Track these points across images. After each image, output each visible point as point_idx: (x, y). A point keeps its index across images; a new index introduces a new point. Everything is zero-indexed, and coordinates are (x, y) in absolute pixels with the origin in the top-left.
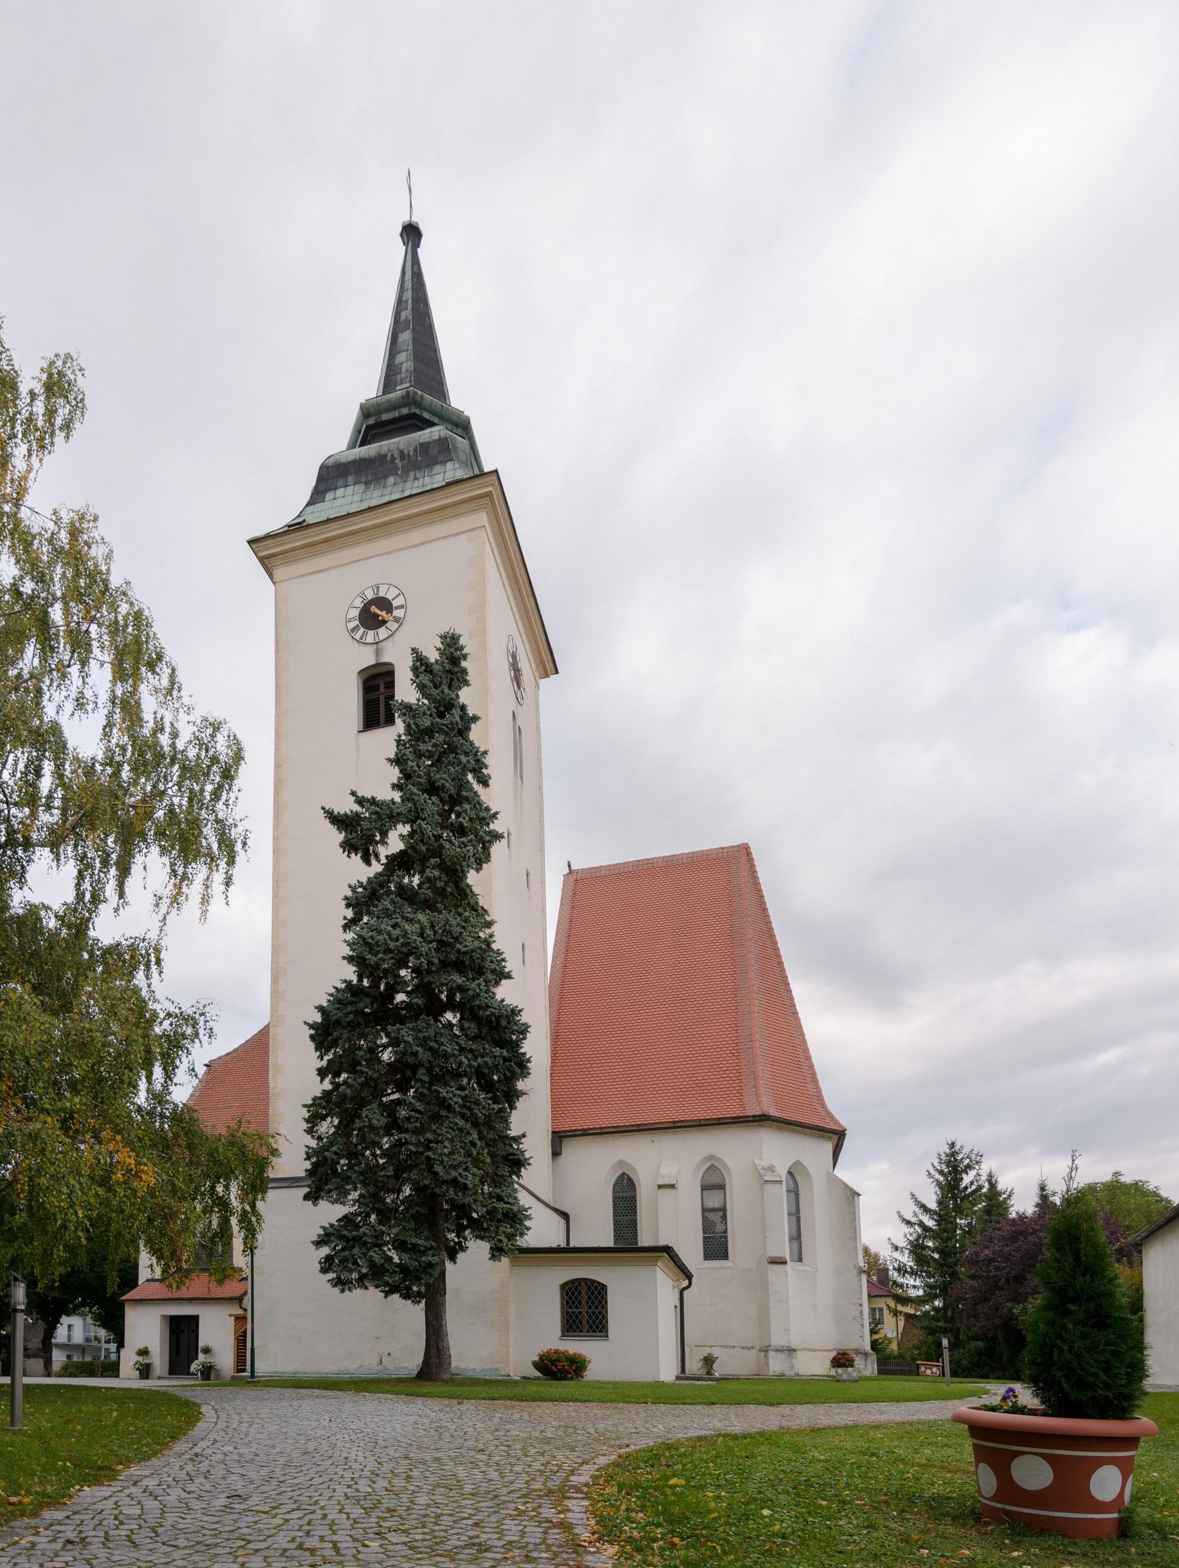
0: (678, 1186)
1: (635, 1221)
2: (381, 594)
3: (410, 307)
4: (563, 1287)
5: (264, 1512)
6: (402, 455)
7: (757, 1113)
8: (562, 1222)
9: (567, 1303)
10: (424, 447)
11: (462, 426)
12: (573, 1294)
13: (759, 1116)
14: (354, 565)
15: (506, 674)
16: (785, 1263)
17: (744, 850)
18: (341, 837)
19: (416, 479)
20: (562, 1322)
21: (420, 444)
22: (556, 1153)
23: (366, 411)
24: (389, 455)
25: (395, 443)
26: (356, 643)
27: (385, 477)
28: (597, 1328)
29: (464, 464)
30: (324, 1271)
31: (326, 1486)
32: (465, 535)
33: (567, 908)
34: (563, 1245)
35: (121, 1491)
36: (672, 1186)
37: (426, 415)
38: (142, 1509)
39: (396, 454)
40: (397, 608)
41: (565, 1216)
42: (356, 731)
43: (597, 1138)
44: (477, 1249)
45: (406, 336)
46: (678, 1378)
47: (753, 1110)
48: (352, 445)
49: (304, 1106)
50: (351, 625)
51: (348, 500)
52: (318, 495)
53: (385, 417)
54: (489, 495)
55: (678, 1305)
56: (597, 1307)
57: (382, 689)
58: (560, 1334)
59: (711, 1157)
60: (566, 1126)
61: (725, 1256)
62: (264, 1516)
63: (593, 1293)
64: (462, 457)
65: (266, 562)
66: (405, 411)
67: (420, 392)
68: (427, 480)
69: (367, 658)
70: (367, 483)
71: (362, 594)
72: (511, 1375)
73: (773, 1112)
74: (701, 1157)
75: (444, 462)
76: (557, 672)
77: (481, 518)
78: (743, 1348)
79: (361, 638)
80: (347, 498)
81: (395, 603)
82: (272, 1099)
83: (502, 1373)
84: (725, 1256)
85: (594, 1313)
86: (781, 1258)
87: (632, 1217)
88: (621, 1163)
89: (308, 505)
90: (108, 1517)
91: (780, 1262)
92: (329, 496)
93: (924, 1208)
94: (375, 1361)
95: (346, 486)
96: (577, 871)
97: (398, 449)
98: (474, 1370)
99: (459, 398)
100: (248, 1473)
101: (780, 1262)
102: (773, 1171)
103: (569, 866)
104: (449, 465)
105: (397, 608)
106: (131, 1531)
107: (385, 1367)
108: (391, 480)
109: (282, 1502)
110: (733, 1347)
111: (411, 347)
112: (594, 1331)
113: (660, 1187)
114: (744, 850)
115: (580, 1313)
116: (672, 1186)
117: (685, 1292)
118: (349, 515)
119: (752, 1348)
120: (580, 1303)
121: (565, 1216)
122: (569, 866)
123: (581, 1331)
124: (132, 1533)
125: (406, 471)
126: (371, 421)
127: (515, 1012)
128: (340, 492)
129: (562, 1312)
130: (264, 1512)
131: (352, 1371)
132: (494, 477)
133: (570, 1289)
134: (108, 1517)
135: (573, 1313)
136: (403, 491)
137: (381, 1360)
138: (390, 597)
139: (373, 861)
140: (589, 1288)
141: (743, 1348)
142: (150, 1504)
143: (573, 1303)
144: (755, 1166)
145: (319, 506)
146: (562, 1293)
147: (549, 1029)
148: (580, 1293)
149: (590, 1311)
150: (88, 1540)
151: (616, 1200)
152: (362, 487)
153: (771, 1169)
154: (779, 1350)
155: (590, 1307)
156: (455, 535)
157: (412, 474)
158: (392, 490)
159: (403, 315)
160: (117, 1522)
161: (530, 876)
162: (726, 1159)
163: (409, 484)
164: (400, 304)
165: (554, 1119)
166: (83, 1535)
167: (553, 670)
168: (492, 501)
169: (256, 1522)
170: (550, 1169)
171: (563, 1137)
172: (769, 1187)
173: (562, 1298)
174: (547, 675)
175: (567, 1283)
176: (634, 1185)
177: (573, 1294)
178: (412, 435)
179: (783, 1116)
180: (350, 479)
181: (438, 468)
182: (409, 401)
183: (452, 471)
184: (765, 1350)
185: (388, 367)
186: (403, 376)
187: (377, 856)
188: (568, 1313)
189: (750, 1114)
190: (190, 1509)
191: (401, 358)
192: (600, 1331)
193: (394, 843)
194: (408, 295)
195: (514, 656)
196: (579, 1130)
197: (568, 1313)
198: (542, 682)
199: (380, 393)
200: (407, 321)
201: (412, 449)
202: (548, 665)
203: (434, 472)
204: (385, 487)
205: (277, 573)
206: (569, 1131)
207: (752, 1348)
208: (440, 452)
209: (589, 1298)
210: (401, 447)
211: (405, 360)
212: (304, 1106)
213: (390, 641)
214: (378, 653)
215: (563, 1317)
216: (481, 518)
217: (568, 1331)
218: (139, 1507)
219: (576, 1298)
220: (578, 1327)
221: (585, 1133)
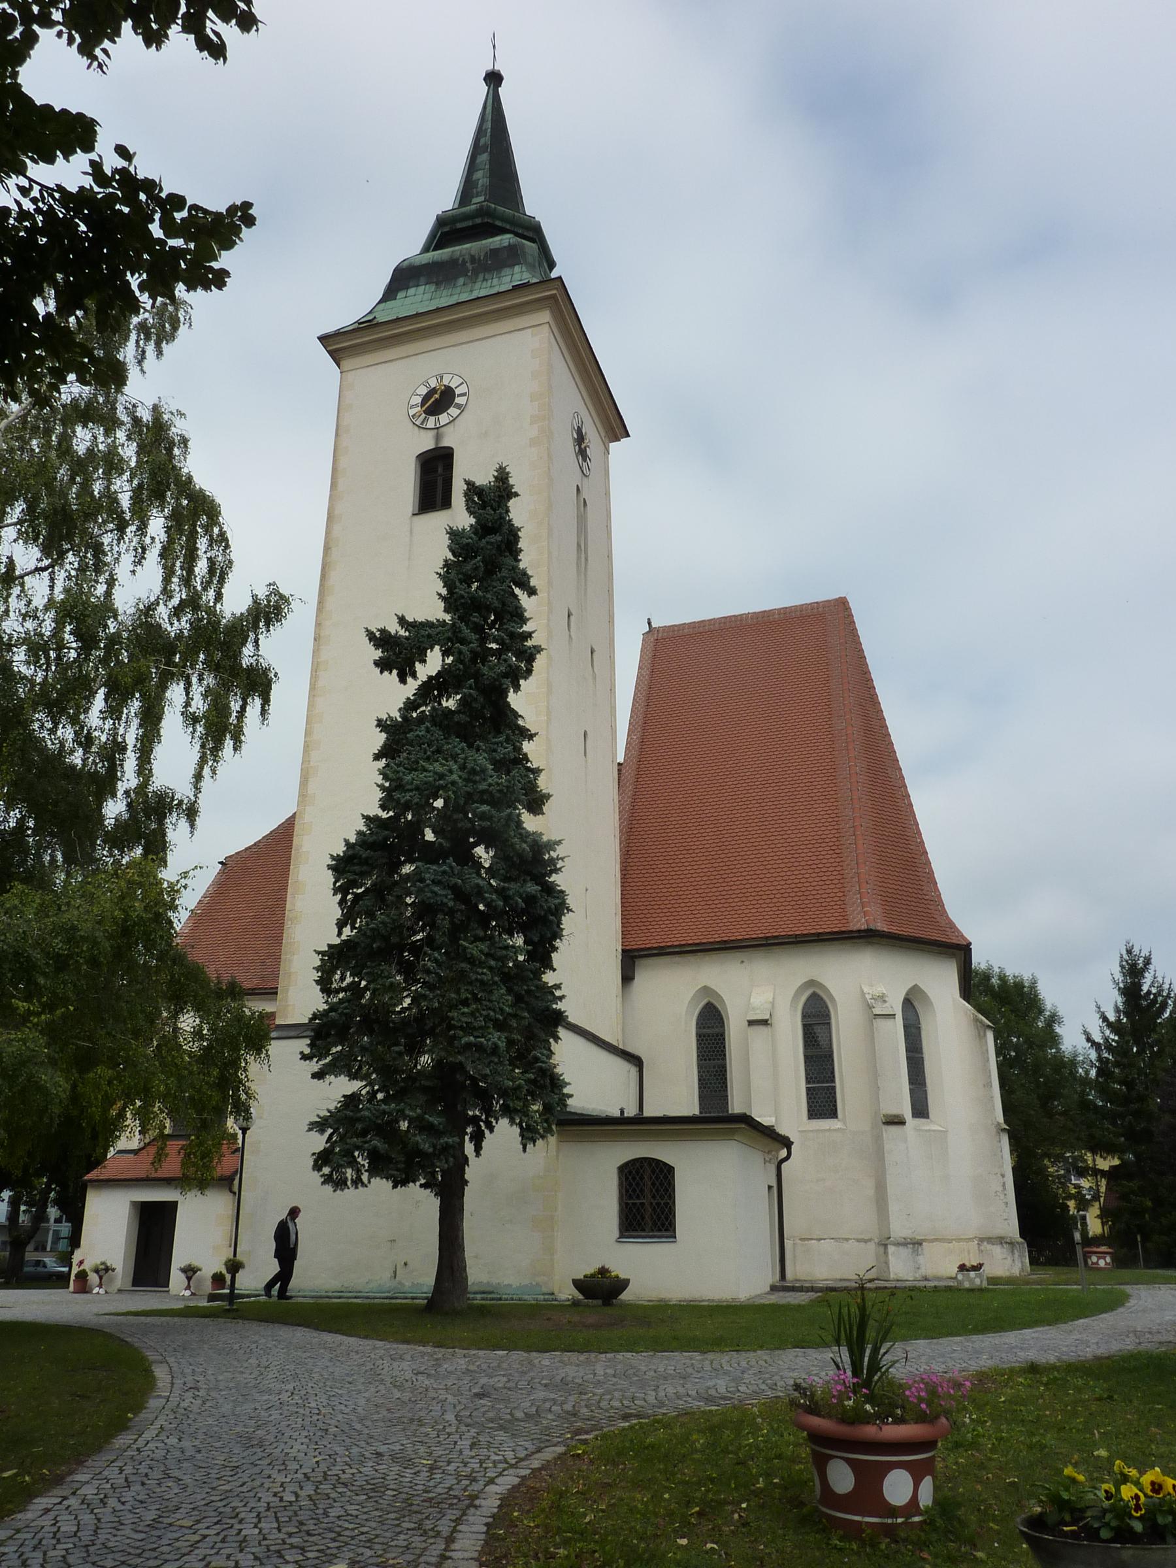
0: (774, 1021)
1: (724, 1067)
2: (445, 382)
3: (489, 134)
4: (621, 1169)
5: (187, 1527)
6: (473, 258)
7: (863, 928)
8: (634, 1071)
9: (627, 1191)
10: (494, 253)
11: (533, 232)
12: (634, 1179)
13: (864, 931)
14: (419, 356)
15: (570, 448)
16: (902, 1122)
17: (842, 605)
18: (378, 654)
19: (485, 280)
20: (620, 1218)
21: (491, 250)
22: (627, 978)
23: (441, 221)
24: (461, 259)
25: (467, 249)
26: (416, 428)
27: (456, 278)
28: (663, 1225)
29: (531, 267)
30: (317, 1167)
31: (252, 1494)
32: (530, 330)
33: (646, 672)
34: (631, 1112)
35: (60, 1503)
36: (764, 1022)
37: (498, 223)
38: (79, 1525)
39: (467, 258)
40: (459, 395)
41: (636, 1061)
42: (410, 514)
43: (677, 958)
44: (504, 1133)
45: (484, 158)
46: (774, 1288)
47: (858, 923)
48: (426, 249)
49: (318, 953)
50: (412, 412)
51: (418, 298)
52: (390, 293)
53: (459, 226)
54: (553, 297)
55: (774, 1184)
56: (662, 1197)
57: (440, 470)
58: (616, 1234)
59: (812, 983)
60: (637, 943)
61: (832, 1113)
62: (187, 1531)
63: (657, 1178)
64: (530, 259)
65: (337, 356)
66: (478, 221)
67: (493, 206)
68: (495, 281)
69: (426, 443)
70: (438, 284)
71: (426, 383)
72: (556, 1292)
73: (881, 926)
74: (792, 993)
75: (512, 266)
76: (628, 435)
77: (545, 316)
78: (859, 1240)
79: (422, 424)
80: (418, 299)
81: (457, 392)
82: (288, 924)
83: (545, 1290)
84: (832, 1113)
85: (658, 1204)
86: (897, 1116)
87: (720, 1062)
88: (706, 990)
89: (380, 302)
90: (47, 1535)
91: (896, 1121)
92: (401, 295)
93: (1105, 1019)
94: (388, 1274)
95: (418, 286)
96: (658, 629)
97: (470, 254)
98: (510, 1286)
99: (534, 203)
100: (185, 1477)
101: (896, 1121)
102: (885, 1001)
103: (649, 623)
104: (517, 268)
105: (459, 395)
106: (66, 1550)
107: (400, 1283)
108: (461, 281)
109: (207, 1514)
110: (847, 1240)
111: (487, 167)
112: (660, 1230)
113: (751, 1023)
114: (842, 605)
115: (642, 1204)
116: (764, 1022)
117: (784, 1165)
118: (418, 315)
119: (870, 1240)
120: (642, 1191)
121: (636, 1061)
122: (649, 623)
123: (643, 1230)
124: (68, 1553)
125: (476, 273)
126: (446, 229)
127: (551, 845)
128: (412, 291)
129: (620, 1204)
130: (187, 1527)
131: (359, 1288)
132: (559, 283)
133: (630, 1172)
134: (47, 1535)
135: (634, 1204)
136: (471, 291)
137: (395, 1272)
138: (453, 385)
139: (409, 680)
140: (653, 1172)
141: (859, 1240)
142: (87, 1518)
143: (634, 1190)
144: (863, 994)
145: (390, 304)
146: (620, 1178)
147: (617, 825)
148: (642, 1178)
149: (654, 1202)
150: (29, 1562)
151: (701, 1038)
152: (433, 287)
153: (882, 998)
154: (904, 1243)
155: (654, 1197)
156: (519, 330)
157: (481, 277)
158: (460, 293)
159: (482, 141)
160: (54, 1542)
161: (595, 654)
162: (829, 985)
163: (478, 285)
164: (480, 132)
165: (625, 934)
166: (24, 1557)
167: (624, 434)
168: (557, 301)
169: (177, 1540)
170: (620, 999)
171: (636, 957)
172: (880, 1023)
173: (621, 1185)
174: (617, 439)
175: (627, 1164)
176: (722, 1019)
177: (634, 1179)
178: (484, 242)
179: (894, 930)
180: (423, 280)
181: (507, 271)
182: (481, 212)
183: (519, 275)
184: (884, 1244)
185: (465, 181)
186: (479, 190)
187: (414, 675)
188: (627, 1204)
189: (855, 929)
190: (122, 1524)
191: (478, 175)
192: (666, 1230)
193: (433, 662)
194: (489, 117)
195: (579, 431)
196: (655, 948)
197: (627, 1204)
198: (613, 446)
199: (456, 206)
200: (485, 145)
201: (482, 255)
202: (616, 428)
203: (503, 274)
204: (455, 286)
205: (343, 363)
206: (642, 950)
207: (870, 1240)
208: (511, 257)
209: (653, 1184)
210: (473, 253)
211: (481, 177)
212: (318, 953)
213: (451, 426)
214: (438, 438)
215: (621, 1211)
216: (545, 316)
217: (627, 1230)
218: (75, 1522)
219: (638, 1184)
220: (639, 1224)
221: (662, 952)
